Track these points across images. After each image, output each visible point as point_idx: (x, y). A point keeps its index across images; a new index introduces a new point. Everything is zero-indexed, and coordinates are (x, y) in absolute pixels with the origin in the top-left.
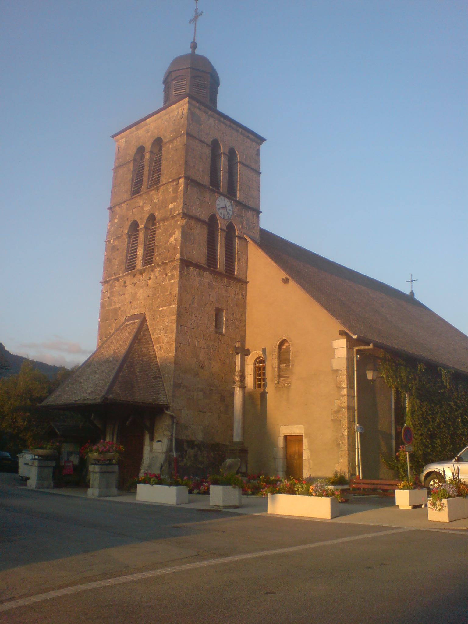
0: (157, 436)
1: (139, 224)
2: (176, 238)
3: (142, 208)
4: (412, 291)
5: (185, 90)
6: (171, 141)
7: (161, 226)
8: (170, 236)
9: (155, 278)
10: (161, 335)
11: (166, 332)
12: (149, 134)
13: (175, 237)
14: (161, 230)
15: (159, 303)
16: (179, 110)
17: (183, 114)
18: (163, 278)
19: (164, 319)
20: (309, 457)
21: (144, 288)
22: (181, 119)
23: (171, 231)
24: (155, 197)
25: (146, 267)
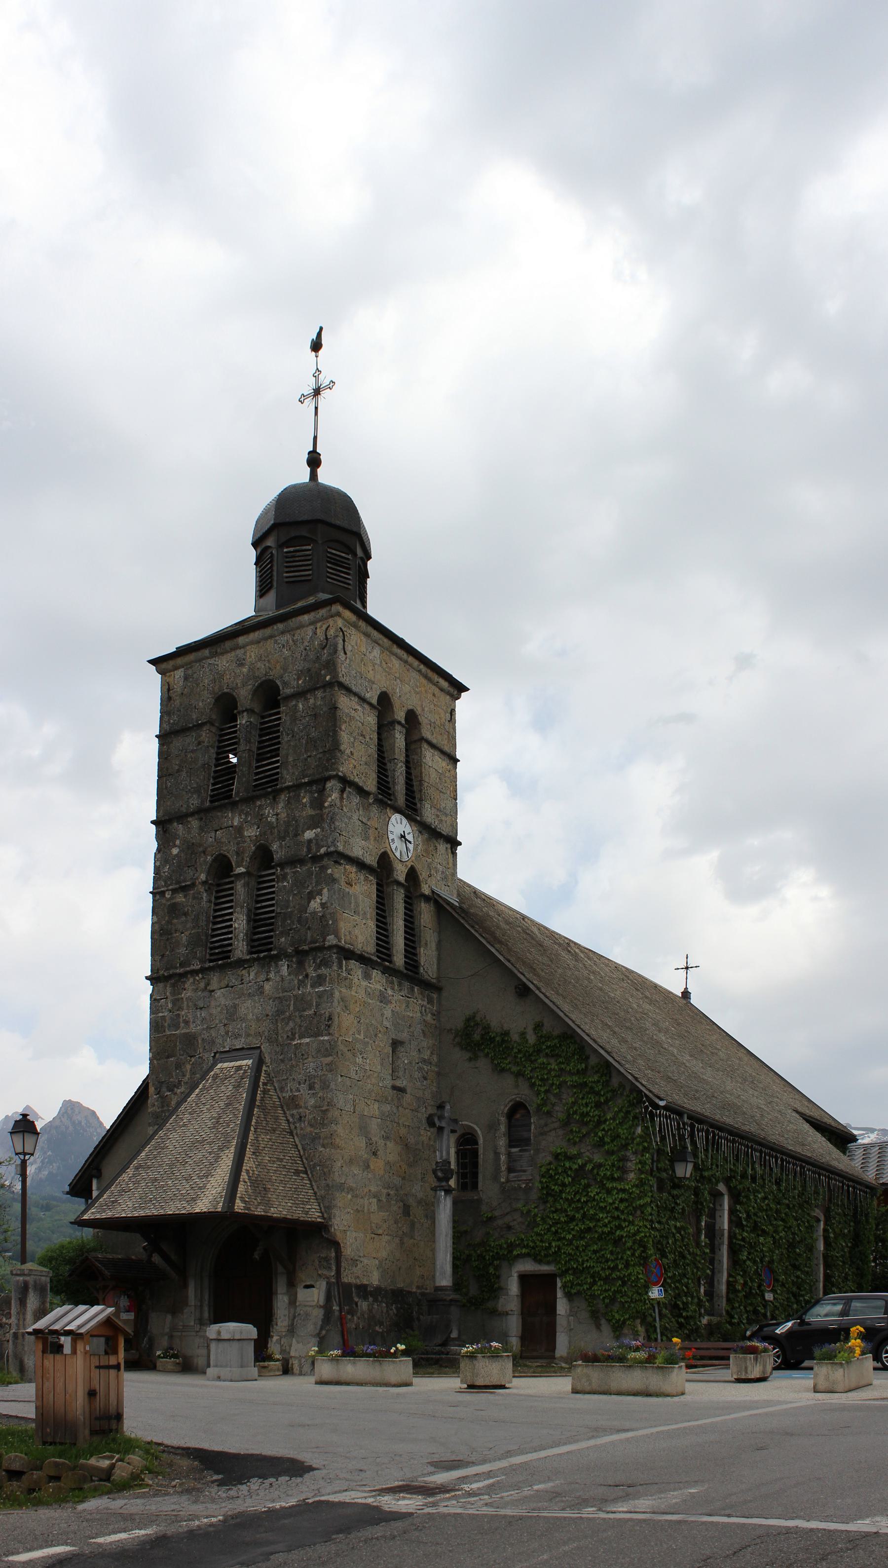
0: (304, 1276)
1: (233, 864)
2: (325, 903)
3: (239, 830)
4: (686, 988)
5: (310, 572)
6: (301, 694)
7: (286, 874)
8: (311, 896)
9: (278, 979)
10: (300, 1091)
11: (311, 1087)
12: (245, 670)
13: (321, 900)
14: (288, 883)
15: (292, 1029)
16: (316, 628)
17: (327, 639)
18: (299, 980)
19: (305, 1061)
20: (568, 1311)
21: (256, 998)
22: (323, 649)
23: (313, 888)
24: (269, 812)
25: (258, 956)
